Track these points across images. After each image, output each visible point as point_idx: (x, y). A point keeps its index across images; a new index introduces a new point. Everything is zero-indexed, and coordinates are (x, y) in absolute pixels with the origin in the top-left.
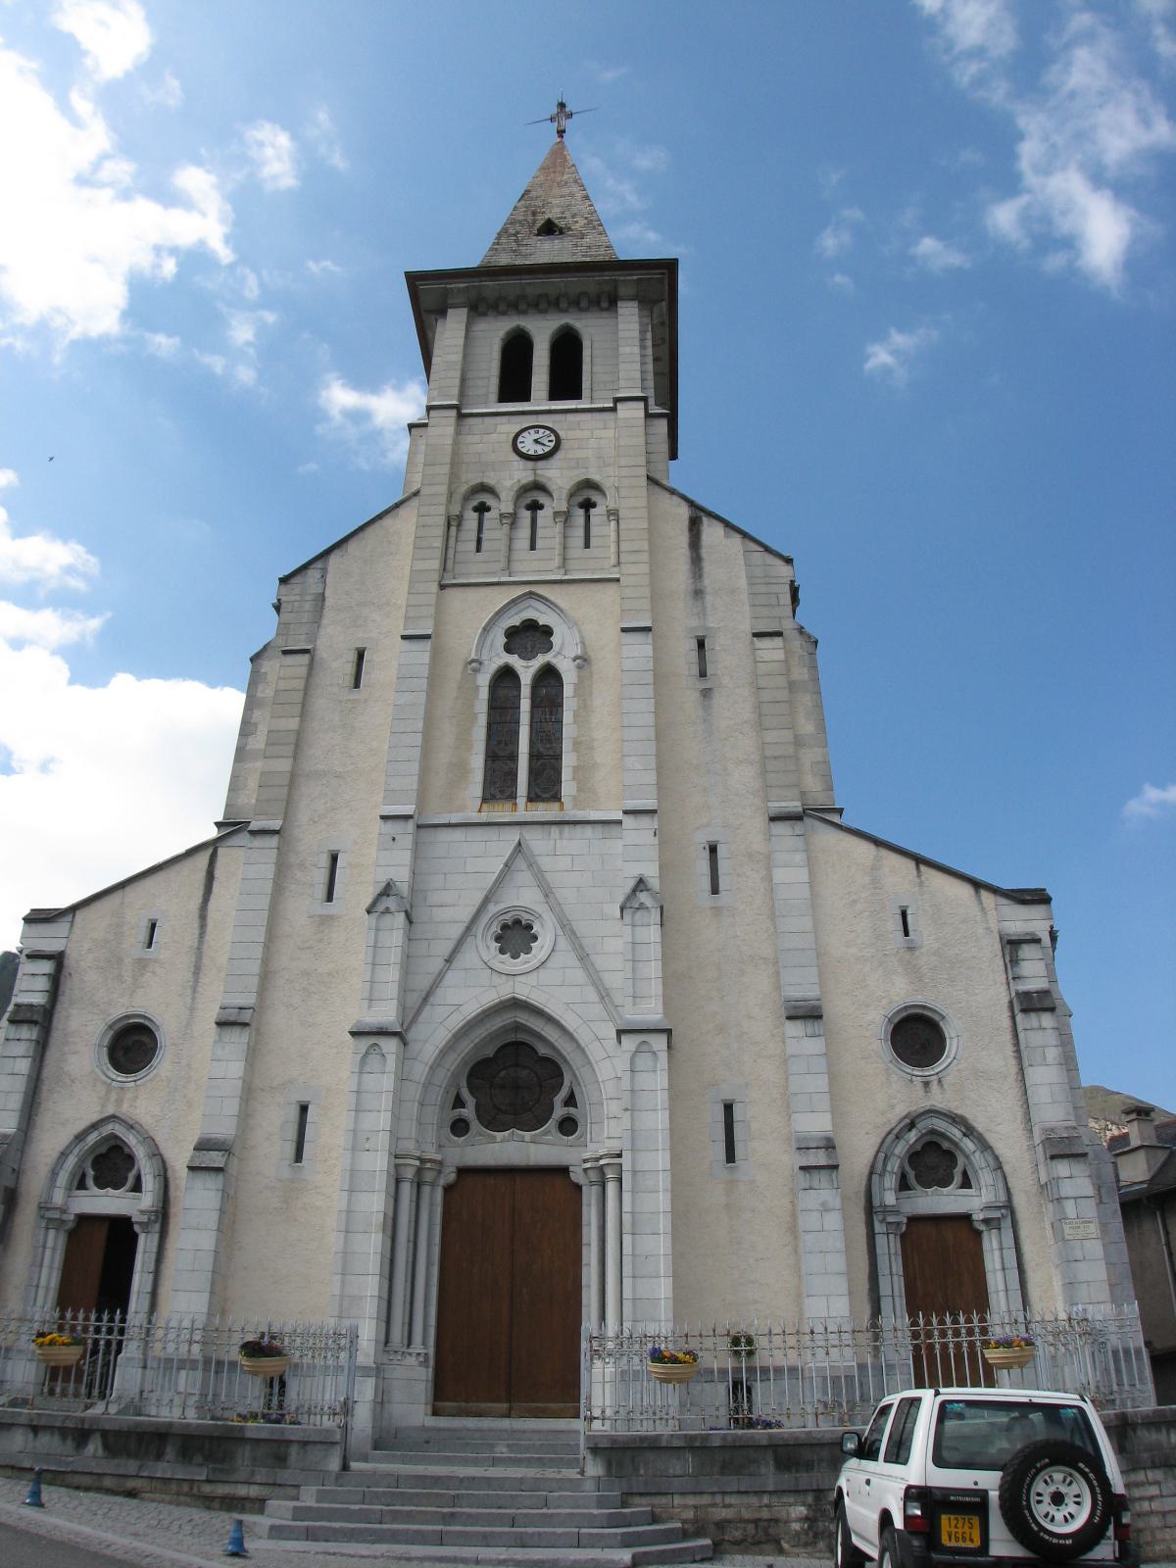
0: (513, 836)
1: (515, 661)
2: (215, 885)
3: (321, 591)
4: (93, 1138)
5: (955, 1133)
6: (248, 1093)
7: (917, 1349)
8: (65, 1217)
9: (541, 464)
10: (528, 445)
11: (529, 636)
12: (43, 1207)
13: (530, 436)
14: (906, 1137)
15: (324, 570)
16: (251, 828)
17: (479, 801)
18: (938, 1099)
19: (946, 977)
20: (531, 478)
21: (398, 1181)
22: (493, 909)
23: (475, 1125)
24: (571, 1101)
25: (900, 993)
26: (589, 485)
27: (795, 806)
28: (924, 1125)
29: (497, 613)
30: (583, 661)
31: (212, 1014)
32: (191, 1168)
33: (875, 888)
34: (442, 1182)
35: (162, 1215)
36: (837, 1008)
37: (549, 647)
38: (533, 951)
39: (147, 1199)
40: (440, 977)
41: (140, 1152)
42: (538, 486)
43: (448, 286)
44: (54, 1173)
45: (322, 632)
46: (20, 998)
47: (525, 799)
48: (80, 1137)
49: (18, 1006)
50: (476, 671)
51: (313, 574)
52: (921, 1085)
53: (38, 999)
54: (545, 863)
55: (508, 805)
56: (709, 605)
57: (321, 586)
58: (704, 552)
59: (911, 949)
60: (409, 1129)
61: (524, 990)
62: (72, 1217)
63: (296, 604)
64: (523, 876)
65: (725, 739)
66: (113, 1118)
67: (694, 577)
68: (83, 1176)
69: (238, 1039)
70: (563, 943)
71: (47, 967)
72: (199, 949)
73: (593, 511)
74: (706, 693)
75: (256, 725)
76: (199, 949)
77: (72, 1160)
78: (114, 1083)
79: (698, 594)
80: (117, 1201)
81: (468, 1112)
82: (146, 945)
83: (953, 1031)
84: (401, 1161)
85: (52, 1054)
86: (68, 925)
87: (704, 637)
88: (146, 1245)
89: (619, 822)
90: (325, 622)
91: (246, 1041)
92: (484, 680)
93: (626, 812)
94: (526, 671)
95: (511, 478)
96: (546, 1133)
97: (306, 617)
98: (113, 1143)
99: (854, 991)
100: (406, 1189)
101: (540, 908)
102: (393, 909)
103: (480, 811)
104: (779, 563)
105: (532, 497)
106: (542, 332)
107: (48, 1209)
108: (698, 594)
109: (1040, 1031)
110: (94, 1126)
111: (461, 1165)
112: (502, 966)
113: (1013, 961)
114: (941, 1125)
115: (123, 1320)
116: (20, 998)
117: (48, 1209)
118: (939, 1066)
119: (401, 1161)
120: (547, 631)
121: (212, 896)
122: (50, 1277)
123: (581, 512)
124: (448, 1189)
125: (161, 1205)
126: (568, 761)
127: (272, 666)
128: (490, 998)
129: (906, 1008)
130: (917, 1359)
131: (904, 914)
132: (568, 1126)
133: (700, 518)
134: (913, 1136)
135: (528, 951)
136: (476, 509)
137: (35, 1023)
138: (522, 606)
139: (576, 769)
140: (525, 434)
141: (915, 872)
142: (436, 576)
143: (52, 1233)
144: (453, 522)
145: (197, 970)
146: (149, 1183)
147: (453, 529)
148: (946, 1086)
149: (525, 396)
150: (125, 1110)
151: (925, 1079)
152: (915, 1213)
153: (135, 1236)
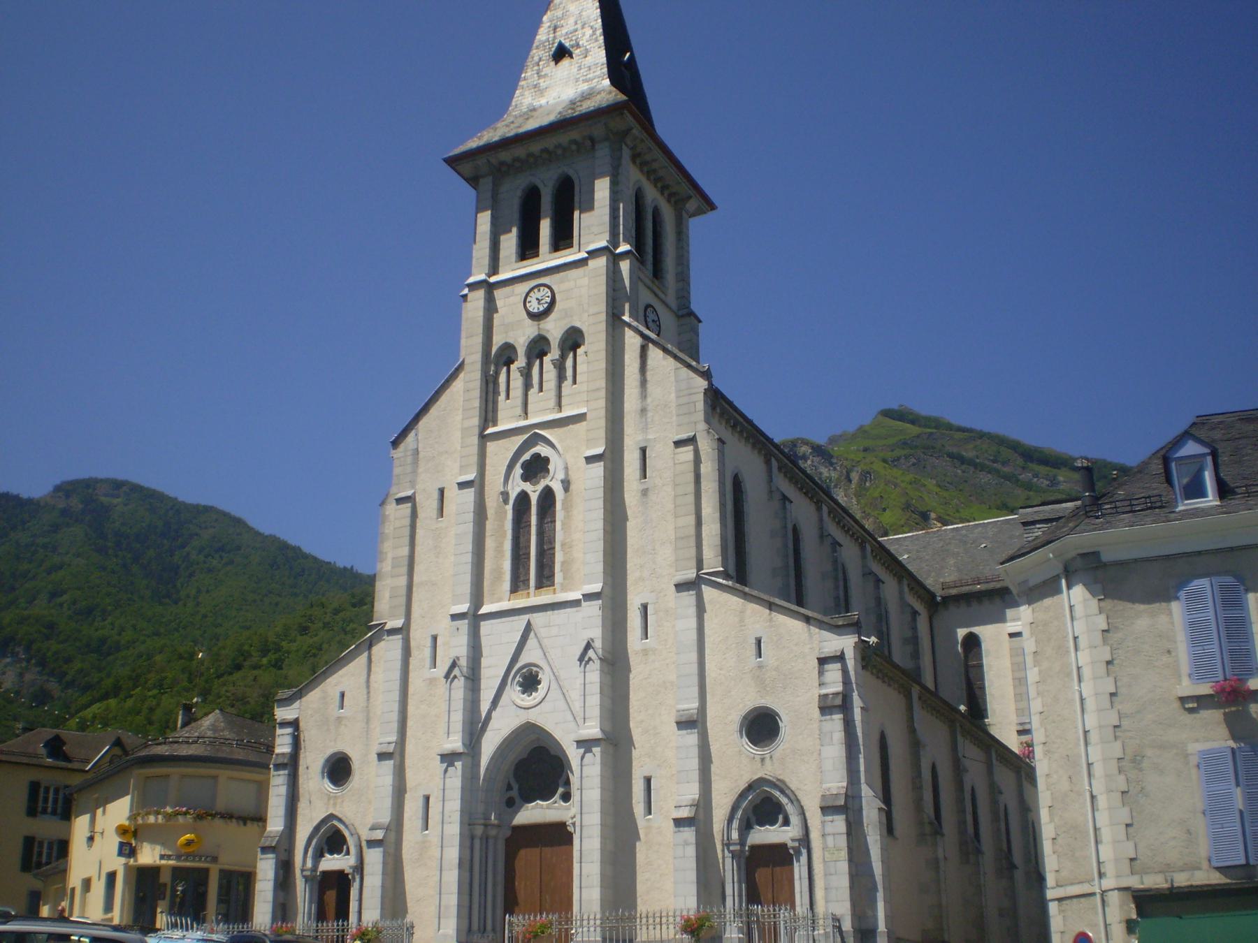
1: (527, 487)
2: (373, 665)
3: (416, 447)
10: (534, 307)
13: (535, 295)
16: (387, 627)
17: (509, 593)
19: (781, 685)
20: (536, 333)
21: (472, 838)
25: (751, 700)
30: (566, 484)
33: (741, 626)
35: (360, 868)
38: (539, 691)
47: (534, 588)
56: (649, 420)
61: (535, 717)
63: (402, 459)
65: (655, 527)
67: (642, 398)
70: (554, 685)
71: (289, 730)
78: (332, 794)
80: (338, 862)
81: (514, 793)
82: (339, 707)
87: (646, 447)
90: (420, 470)
95: (524, 335)
97: (409, 469)
98: (334, 830)
99: (723, 700)
100: (477, 843)
105: (538, 348)
106: (546, 182)
112: (536, 700)
115: (348, 925)
120: (547, 460)
121: (372, 673)
125: (359, 862)
126: (559, 557)
132: (566, 797)
133: (647, 345)
135: (536, 690)
139: (563, 563)
140: (529, 299)
142: (476, 431)
146: (353, 850)
148: (775, 760)
151: (762, 757)
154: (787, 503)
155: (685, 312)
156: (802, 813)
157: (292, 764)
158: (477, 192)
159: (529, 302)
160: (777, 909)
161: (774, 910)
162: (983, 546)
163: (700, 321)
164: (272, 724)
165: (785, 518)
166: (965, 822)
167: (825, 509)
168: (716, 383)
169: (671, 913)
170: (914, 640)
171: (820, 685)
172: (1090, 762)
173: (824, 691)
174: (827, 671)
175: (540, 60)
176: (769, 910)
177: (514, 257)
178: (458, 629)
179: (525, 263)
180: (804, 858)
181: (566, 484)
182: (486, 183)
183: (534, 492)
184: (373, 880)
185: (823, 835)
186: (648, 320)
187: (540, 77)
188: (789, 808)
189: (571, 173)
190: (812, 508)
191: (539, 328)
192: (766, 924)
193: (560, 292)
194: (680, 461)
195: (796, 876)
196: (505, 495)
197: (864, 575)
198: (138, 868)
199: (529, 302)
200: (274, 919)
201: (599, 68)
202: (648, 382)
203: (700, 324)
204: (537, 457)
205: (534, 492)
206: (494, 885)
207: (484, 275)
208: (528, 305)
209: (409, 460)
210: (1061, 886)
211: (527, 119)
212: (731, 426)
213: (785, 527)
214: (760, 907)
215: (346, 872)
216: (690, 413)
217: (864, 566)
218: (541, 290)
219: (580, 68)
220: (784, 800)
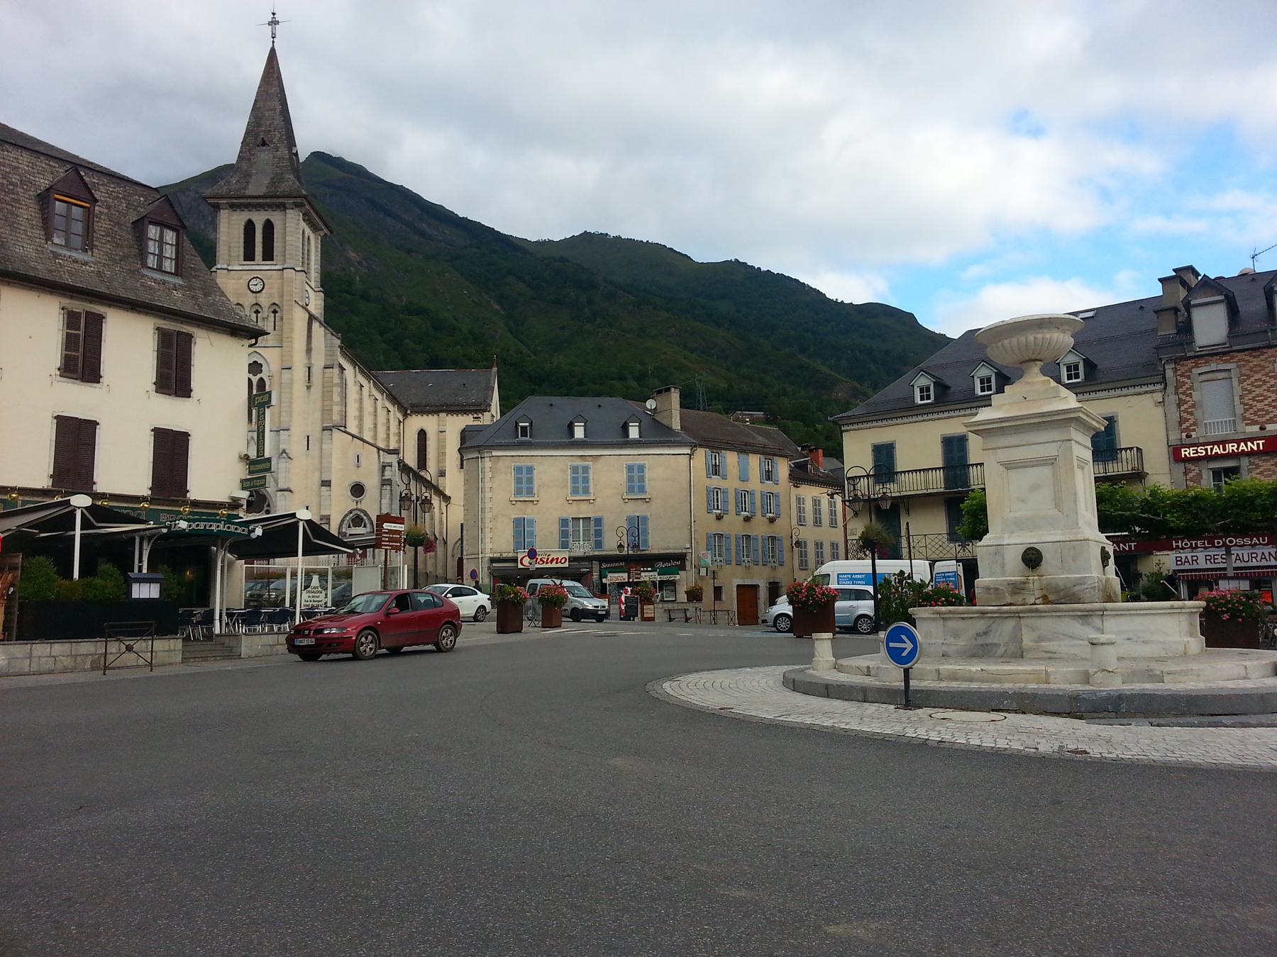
5: (362, 515)
13: (254, 282)
24: (269, 506)
25: (355, 478)
28: (354, 513)
43: (220, 202)
59: (358, 467)
68: (350, 524)
73: (277, 314)
94: (255, 380)
114: (359, 513)
123: (273, 315)
134: (351, 515)
219: (274, 157)
220: (365, 518)
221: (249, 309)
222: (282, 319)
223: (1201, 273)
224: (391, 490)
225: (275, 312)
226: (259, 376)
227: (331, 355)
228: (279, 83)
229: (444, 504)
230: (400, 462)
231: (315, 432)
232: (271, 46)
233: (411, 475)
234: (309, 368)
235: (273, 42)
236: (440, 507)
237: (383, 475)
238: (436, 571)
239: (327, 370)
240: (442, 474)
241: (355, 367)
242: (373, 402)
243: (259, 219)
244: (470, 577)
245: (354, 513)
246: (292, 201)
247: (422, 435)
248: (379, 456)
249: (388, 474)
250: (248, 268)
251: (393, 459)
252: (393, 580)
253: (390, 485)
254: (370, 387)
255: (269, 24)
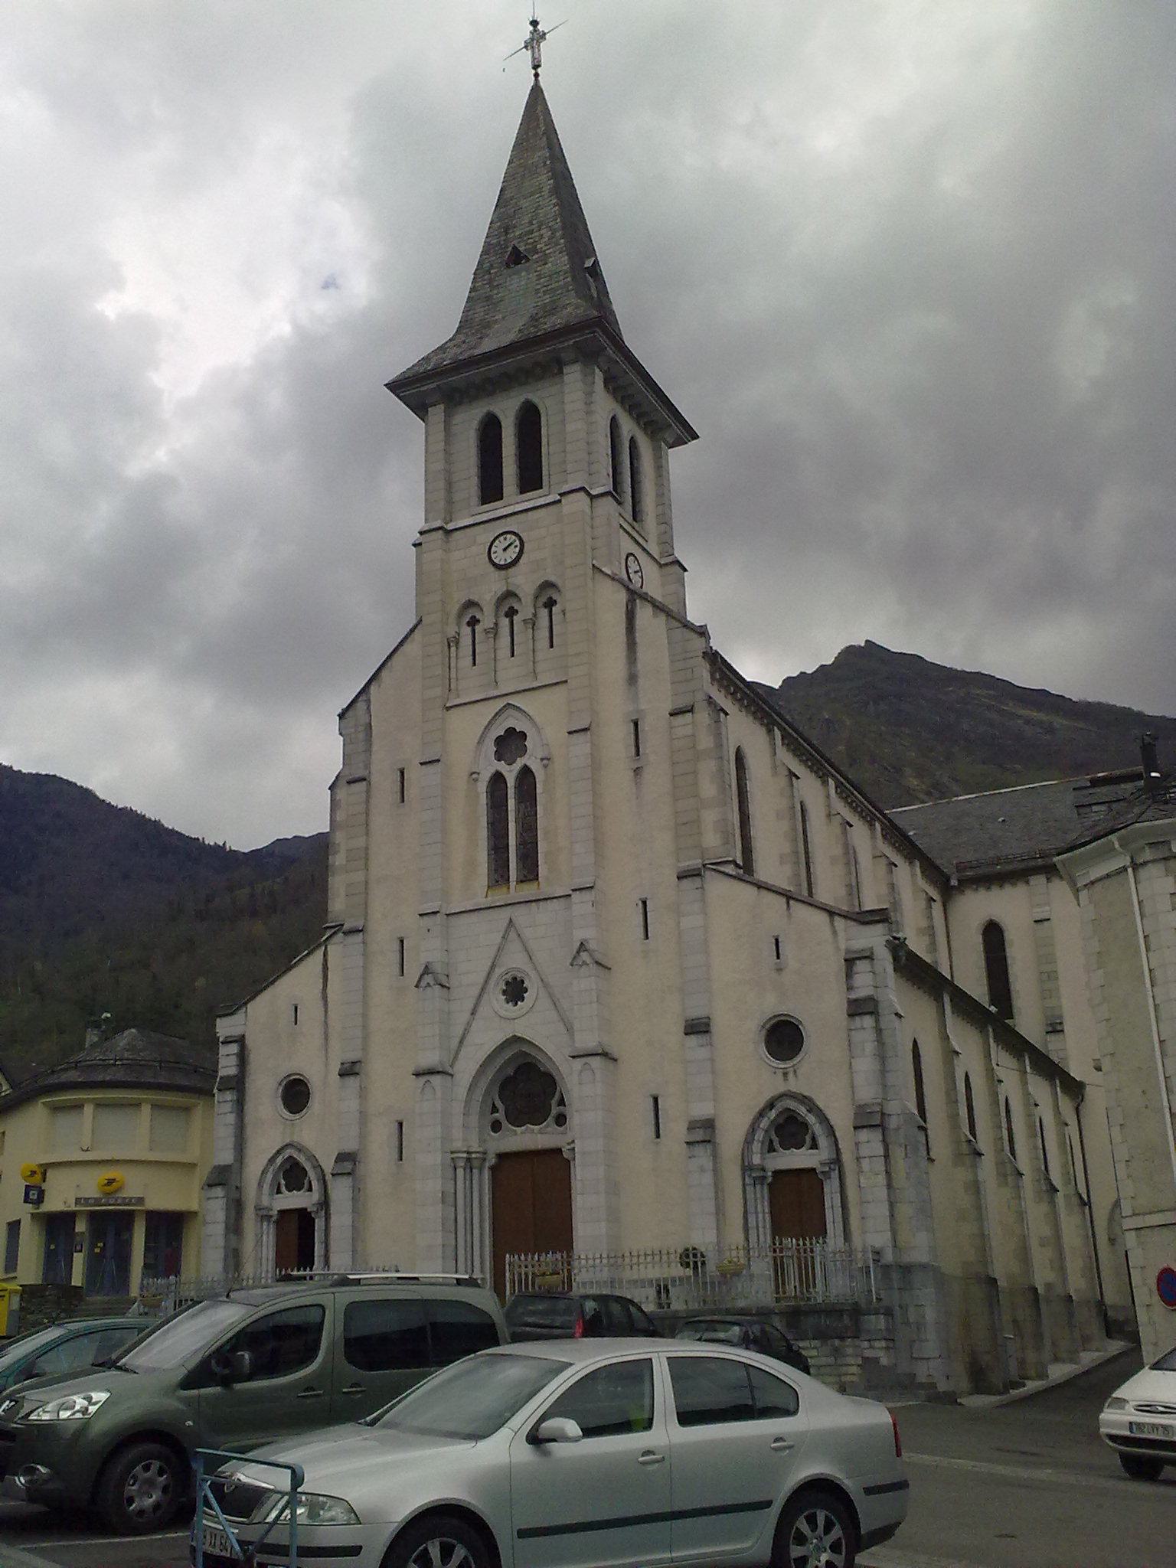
0: (504, 915)
1: (502, 767)
4: (279, 1160)
5: (802, 1110)
6: (363, 1117)
7: (775, 1259)
8: (271, 1213)
9: (511, 571)
10: (500, 558)
11: (510, 743)
12: (258, 1208)
13: (500, 544)
14: (769, 1115)
15: (368, 701)
18: (793, 1085)
20: (505, 589)
22: (498, 971)
23: (505, 1123)
25: (771, 1005)
26: (548, 585)
27: (697, 863)
28: (780, 1106)
29: (497, 714)
31: (335, 1068)
32: (333, 1175)
34: (487, 1164)
35: (325, 1204)
36: (721, 1024)
37: (524, 750)
39: (316, 1196)
40: (469, 1024)
41: (308, 1167)
42: (510, 594)
44: (260, 1185)
45: (373, 757)
46: (222, 1073)
48: (272, 1160)
49: (221, 1078)
50: (476, 780)
51: (361, 705)
52: (781, 1074)
53: (233, 1071)
54: (527, 933)
55: (505, 889)
57: (367, 716)
58: (639, 636)
59: (779, 970)
60: (457, 1133)
61: (521, 1030)
62: (276, 1212)
64: (514, 946)
66: (287, 1146)
68: (771, 1141)
69: (352, 1081)
70: (542, 993)
72: (326, 1022)
74: (637, 771)
75: (339, 844)
76: (326, 1022)
77: (270, 1176)
79: (632, 679)
81: (500, 1115)
83: (809, 1031)
84: (456, 1155)
85: (249, 1107)
86: (244, 1014)
87: (637, 719)
88: (319, 1224)
89: (570, 895)
90: (374, 748)
91: (358, 1084)
92: (482, 787)
93: (573, 890)
94: (511, 773)
96: (547, 1126)
101: (528, 968)
102: (432, 983)
103: (486, 897)
104: (694, 636)
106: (507, 409)
107: (260, 1209)
108: (632, 679)
109: (862, 1031)
110: (279, 1152)
111: (498, 1152)
113: (849, 974)
114: (792, 1104)
116: (222, 1073)
117: (260, 1209)
118: (795, 1061)
119: (456, 1155)
120: (523, 735)
122: (269, 1252)
124: (492, 1169)
127: (342, 793)
128: (501, 1038)
129: (775, 1016)
130: (776, 1264)
131: (777, 941)
132: (561, 1120)
134: (773, 1114)
136: (469, 624)
137: (234, 1089)
138: (504, 716)
140: (493, 549)
141: (785, 906)
143: (265, 1224)
144: (454, 642)
145: (326, 1038)
147: (453, 649)
149: (499, 496)
150: (296, 1139)
151: (785, 1071)
152: (778, 1168)
153: (314, 1220)
154: (794, 779)
155: (670, 559)
156: (831, 1132)
157: (238, 1084)
158: (426, 425)
159: (495, 553)
160: (814, 1242)
161: (811, 1244)
162: (1000, 820)
163: (685, 570)
164: (213, 1043)
165: (793, 796)
166: (1001, 1138)
167: (831, 782)
168: (715, 644)
169: (664, 1252)
170: (931, 931)
171: (848, 989)
172: (1167, 1076)
173: (853, 996)
174: (856, 973)
175: (492, 266)
176: (805, 1244)
177: (475, 499)
178: (429, 930)
179: (487, 507)
180: (836, 1183)
181: (546, 760)
182: (437, 413)
183: (511, 771)
184: (341, 1219)
185: (858, 1159)
186: (630, 571)
187: (492, 288)
188: (817, 1128)
189: (536, 400)
190: (818, 783)
191: (507, 583)
192: (803, 1259)
193: (530, 541)
194: (677, 736)
195: (827, 1204)
196: (473, 775)
197: (874, 857)
198: (48, 1215)
199: (495, 553)
200: (226, 1269)
201: (562, 278)
202: (638, 645)
203: (686, 573)
204: (511, 731)
205: (511, 771)
206: (481, 1221)
207: (439, 521)
208: (493, 556)
209: (361, 736)
210: (1138, 1214)
211: (481, 338)
212: (731, 694)
213: (793, 807)
214: (794, 1240)
215: (309, 1210)
216: (687, 681)
217: (874, 847)
218: (508, 539)
219: (539, 277)
220: (811, 1119)
221: (492, 607)
222: (564, 612)
223: (827, 1537)
224: (879, 1031)
225: (550, 604)
226: (519, 763)
227: (687, 681)
228: (552, 157)
229: (1066, 1105)
230: (897, 947)
231: (664, 888)
232: (532, 83)
233: (947, 999)
234: (636, 724)
235: (536, 75)
236: (1056, 1106)
237: (850, 988)
238: (1065, 1280)
239: (680, 720)
240: (1055, 1028)
241: (770, 731)
242: (838, 830)
243: (507, 409)
244: (1156, 1298)
245: (780, 1106)
246: (571, 342)
247: (993, 934)
248: (835, 933)
249: (864, 982)
250: (485, 517)
251: (874, 938)
252: (911, 1309)
253: (874, 1013)
254: (828, 796)
255: (526, 47)
